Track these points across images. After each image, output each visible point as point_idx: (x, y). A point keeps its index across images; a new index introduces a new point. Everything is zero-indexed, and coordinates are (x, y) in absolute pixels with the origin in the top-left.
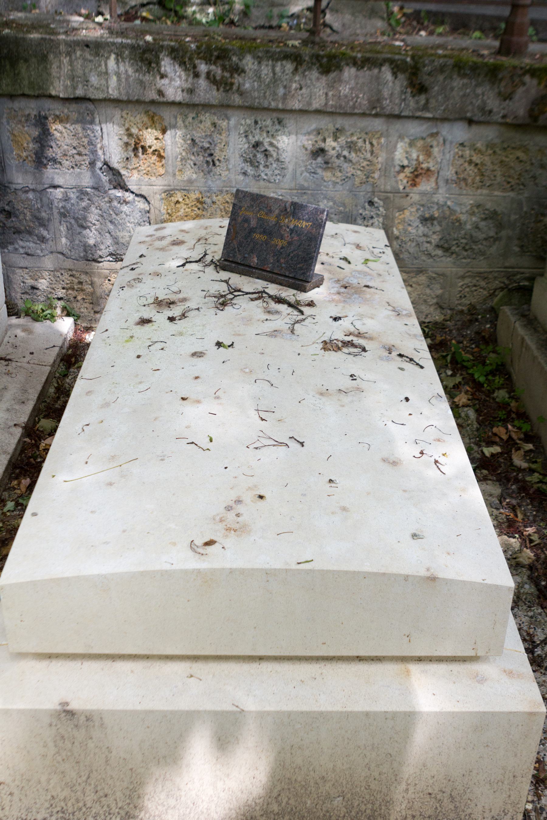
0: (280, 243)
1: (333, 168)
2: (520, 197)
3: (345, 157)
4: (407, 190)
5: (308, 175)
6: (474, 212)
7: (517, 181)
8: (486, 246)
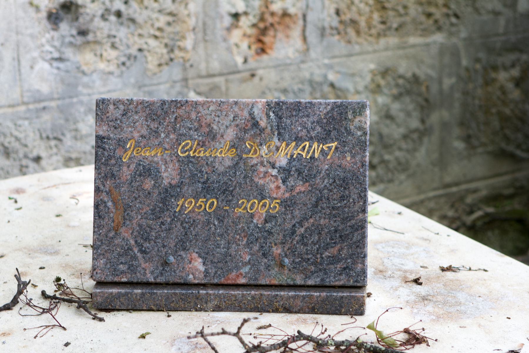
0: (260, 211)
1: (96, 42)
2: (454, 40)
3: (119, 14)
4: (252, 64)
5: (46, 66)
6: (379, 86)
7: (445, 10)
8: (408, 151)
